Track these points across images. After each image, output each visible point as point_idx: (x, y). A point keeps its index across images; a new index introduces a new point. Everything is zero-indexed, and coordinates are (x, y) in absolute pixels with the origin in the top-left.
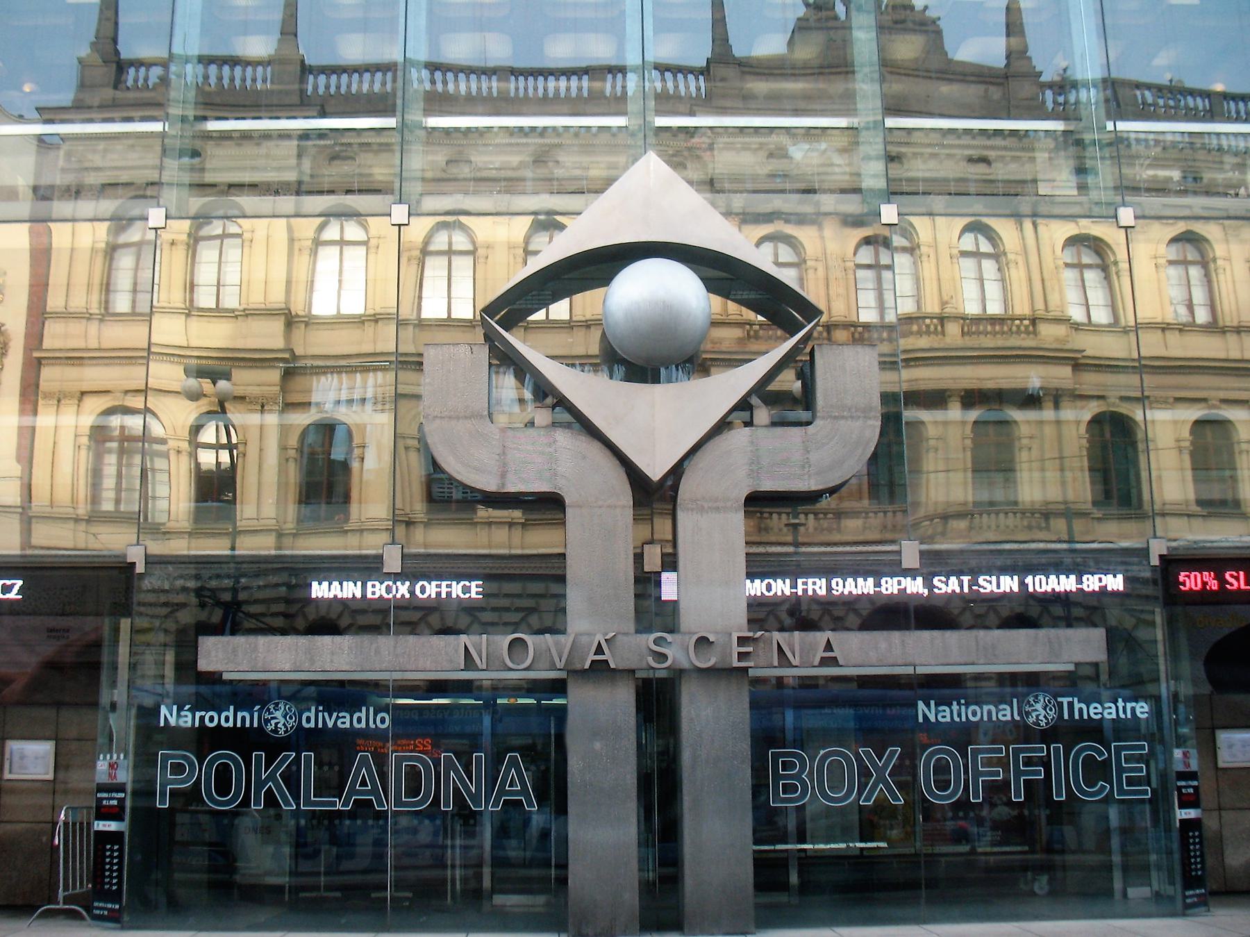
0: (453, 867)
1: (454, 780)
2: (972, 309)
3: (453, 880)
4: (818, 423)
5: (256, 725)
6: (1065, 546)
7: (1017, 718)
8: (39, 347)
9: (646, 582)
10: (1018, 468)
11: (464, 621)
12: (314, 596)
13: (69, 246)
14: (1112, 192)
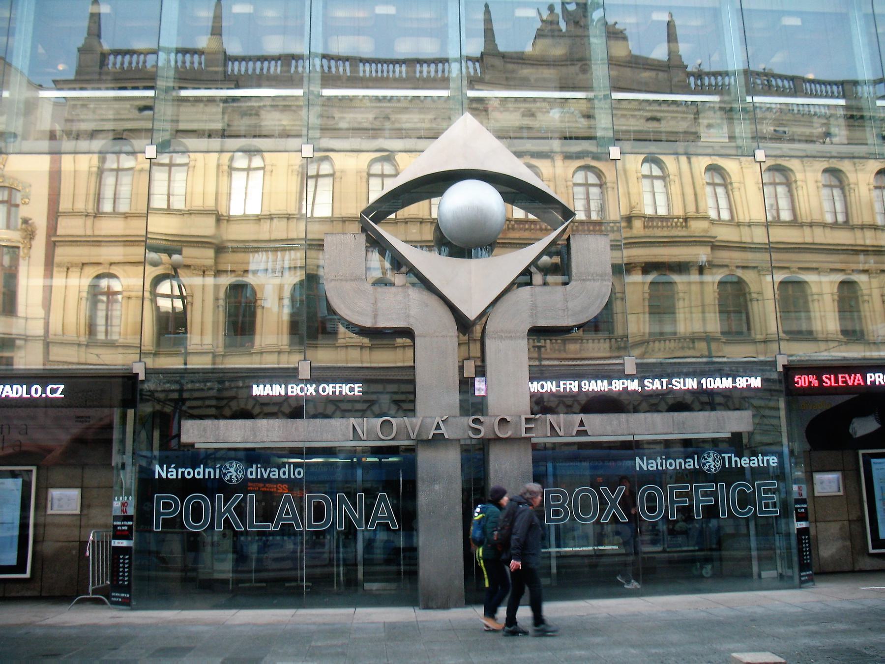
0: (338, 566)
1: (342, 510)
2: (649, 211)
3: (338, 574)
4: (572, 283)
5: (217, 477)
6: (704, 360)
7: (697, 467)
8: (55, 235)
9: (466, 384)
10: (677, 311)
11: (330, 409)
12: (254, 394)
13: (73, 169)
14: (750, 141)
